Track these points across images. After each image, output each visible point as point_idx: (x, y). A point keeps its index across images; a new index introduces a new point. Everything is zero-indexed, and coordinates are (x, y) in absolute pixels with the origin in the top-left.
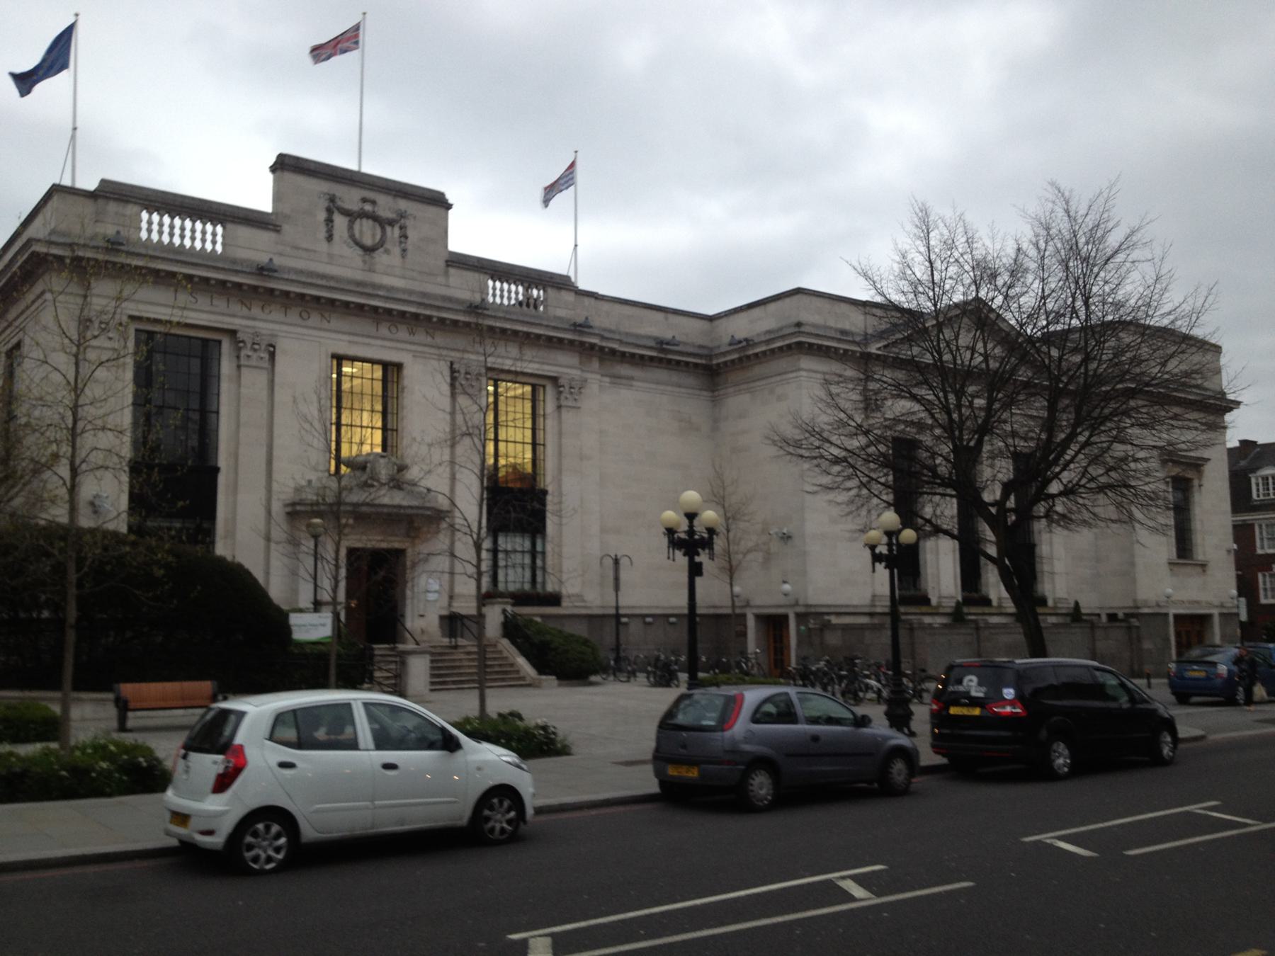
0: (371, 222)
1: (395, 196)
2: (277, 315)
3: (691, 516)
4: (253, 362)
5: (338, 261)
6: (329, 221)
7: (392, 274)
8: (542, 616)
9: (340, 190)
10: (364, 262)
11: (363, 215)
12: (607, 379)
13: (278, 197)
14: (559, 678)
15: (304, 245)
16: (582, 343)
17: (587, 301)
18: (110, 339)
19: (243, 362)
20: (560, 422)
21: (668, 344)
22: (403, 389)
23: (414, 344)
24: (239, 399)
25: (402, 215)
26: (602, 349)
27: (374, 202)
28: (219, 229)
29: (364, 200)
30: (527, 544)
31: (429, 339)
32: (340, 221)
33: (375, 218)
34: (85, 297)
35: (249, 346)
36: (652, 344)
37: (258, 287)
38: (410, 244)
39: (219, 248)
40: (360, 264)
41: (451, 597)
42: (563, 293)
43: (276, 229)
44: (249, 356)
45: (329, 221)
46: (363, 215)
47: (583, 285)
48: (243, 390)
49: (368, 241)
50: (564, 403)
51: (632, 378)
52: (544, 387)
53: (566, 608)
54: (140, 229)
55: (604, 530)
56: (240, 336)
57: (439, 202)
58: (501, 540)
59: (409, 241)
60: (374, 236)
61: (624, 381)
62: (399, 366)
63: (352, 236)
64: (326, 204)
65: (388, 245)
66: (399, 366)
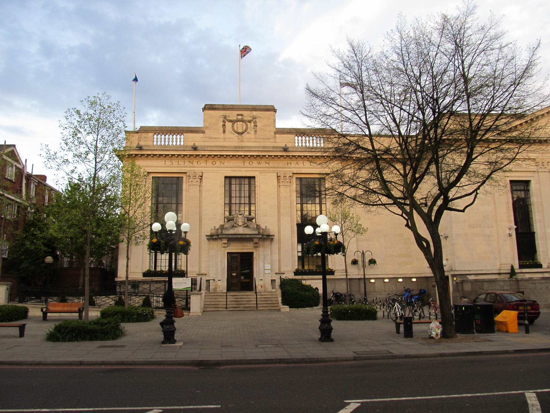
0: (241, 123)
5: (230, 140)
6: (224, 125)
7: (251, 141)
10: (239, 139)
16: (288, 156)
27: (242, 115)
29: (238, 115)
32: (229, 125)
33: (242, 121)
37: (194, 154)
43: (203, 132)
45: (224, 125)
49: (240, 131)
64: (223, 119)
65: (248, 131)
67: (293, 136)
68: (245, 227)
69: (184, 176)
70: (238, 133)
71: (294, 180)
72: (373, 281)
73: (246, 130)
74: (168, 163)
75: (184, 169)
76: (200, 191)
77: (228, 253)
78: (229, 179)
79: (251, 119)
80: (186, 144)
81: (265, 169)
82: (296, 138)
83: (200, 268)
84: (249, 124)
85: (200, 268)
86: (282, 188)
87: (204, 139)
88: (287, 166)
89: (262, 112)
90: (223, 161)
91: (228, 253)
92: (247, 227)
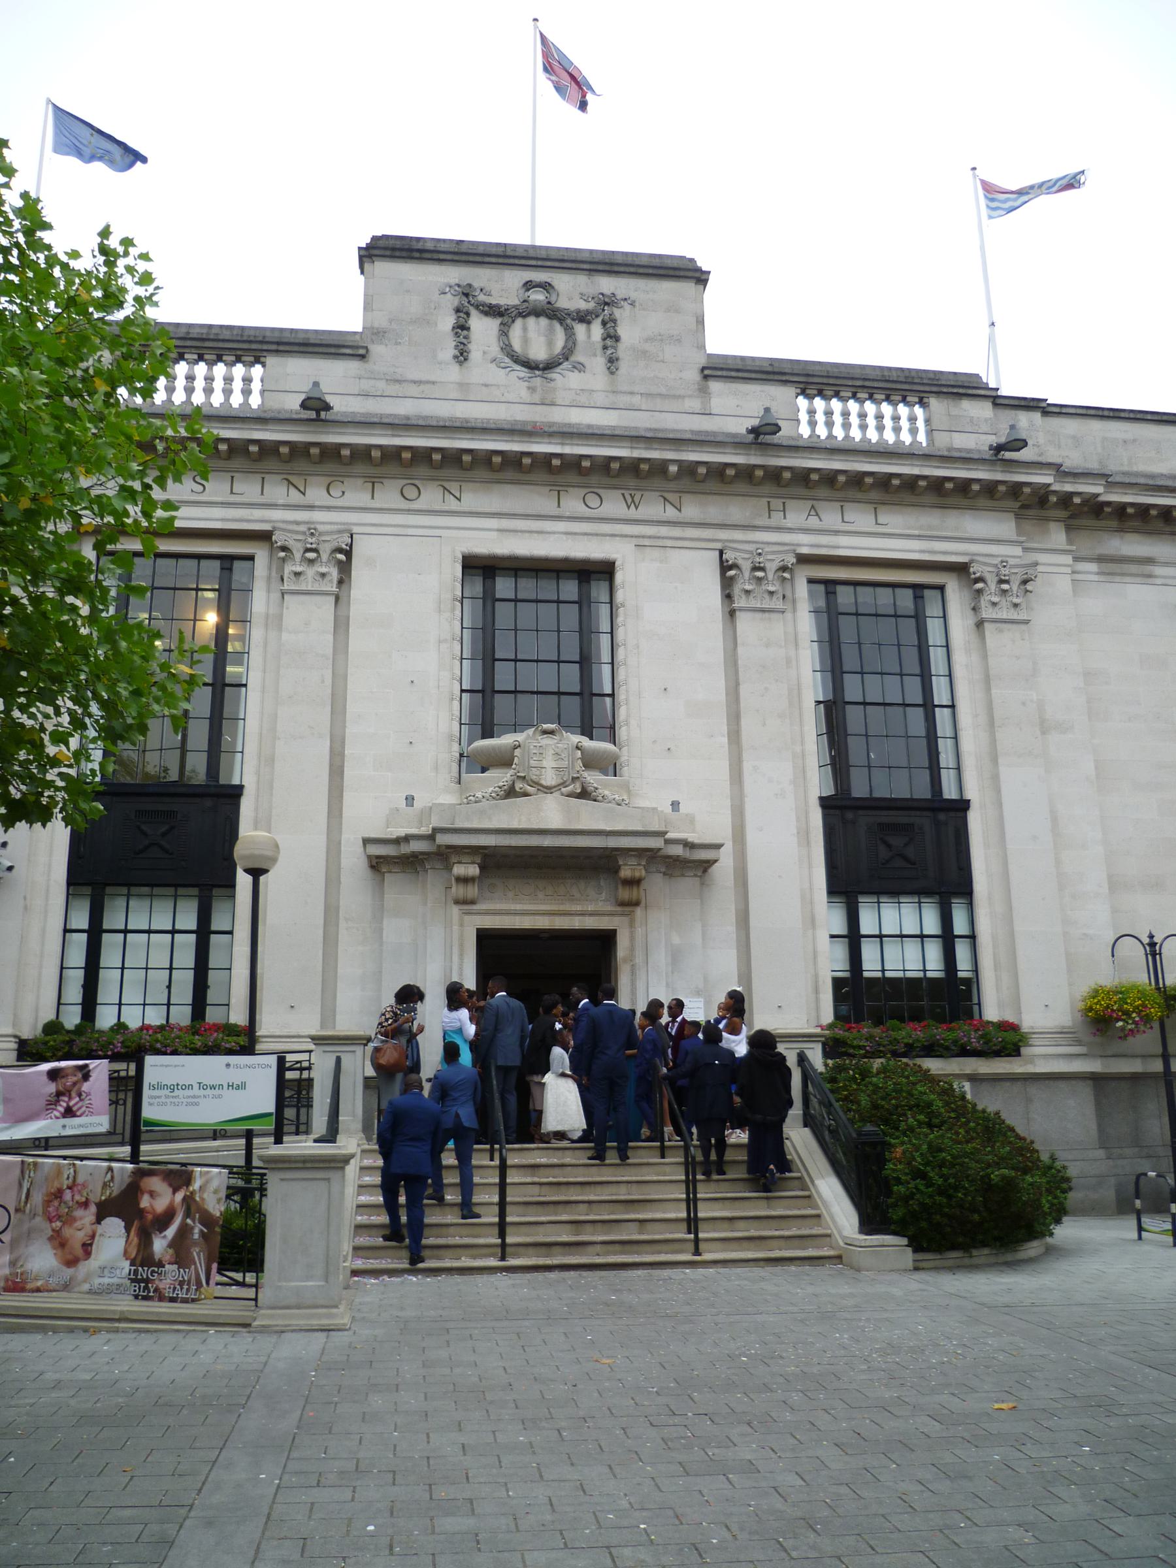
0: (543, 321)
2: (355, 494)
4: (307, 584)
5: (485, 394)
6: (461, 328)
7: (588, 403)
8: (973, 1078)
9: (479, 276)
10: (532, 389)
12: (1093, 567)
14: (918, 1245)
16: (1015, 490)
20: (984, 656)
25: (608, 302)
26: (1066, 500)
27: (546, 286)
29: (529, 285)
30: (931, 923)
31: (671, 513)
32: (483, 329)
33: (550, 312)
35: (298, 555)
37: (310, 450)
38: (623, 350)
40: (525, 394)
42: (966, 404)
43: (362, 356)
45: (461, 328)
49: (539, 353)
50: (987, 613)
51: (1150, 561)
52: (941, 588)
55: (1115, 884)
57: (690, 274)
58: (935, 965)
59: (621, 346)
60: (550, 344)
61: (1133, 568)
62: (605, 571)
63: (508, 350)
64: (456, 302)
65: (578, 357)
66: (605, 571)
67: (791, 391)
69: (261, 555)
70: (530, 365)
71: (802, 589)
73: (567, 354)
75: (258, 513)
76: (341, 625)
78: (481, 569)
79: (591, 305)
81: (664, 531)
82: (802, 402)
83: (328, 1013)
85: (328, 1013)
86: (743, 619)
89: (641, 283)
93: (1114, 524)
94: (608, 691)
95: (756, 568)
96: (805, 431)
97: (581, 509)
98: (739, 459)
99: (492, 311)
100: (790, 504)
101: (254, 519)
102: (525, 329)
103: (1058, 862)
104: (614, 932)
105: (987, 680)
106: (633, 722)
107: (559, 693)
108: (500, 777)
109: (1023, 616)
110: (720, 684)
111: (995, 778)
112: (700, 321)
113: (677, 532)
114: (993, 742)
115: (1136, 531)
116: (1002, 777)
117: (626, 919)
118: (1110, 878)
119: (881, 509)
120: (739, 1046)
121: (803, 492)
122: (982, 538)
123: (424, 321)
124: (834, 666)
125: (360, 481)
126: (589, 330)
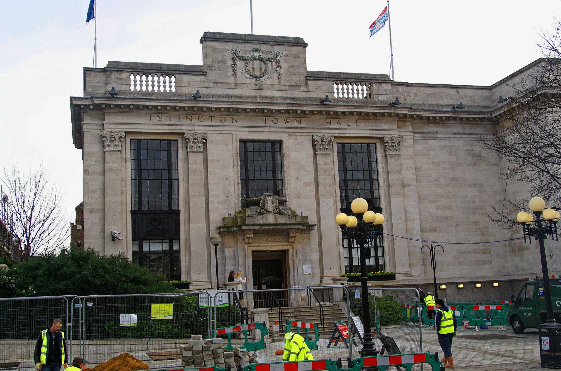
1: (272, 45)
3: (538, 214)
7: (274, 89)
10: (256, 85)
11: (253, 59)
12: (419, 135)
13: (205, 57)
15: (221, 81)
16: (397, 115)
17: (400, 88)
18: (117, 145)
19: (107, 148)
20: (387, 165)
21: (457, 108)
22: (283, 155)
23: (288, 128)
24: (188, 169)
26: (412, 116)
28: (173, 79)
29: (254, 50)
31: (298, 125)
33: (260, 59)
34: (103, 125)
36: (449, 109)
37: (192, 107)
39: (173, 89)
41: (322, 278)
42: (383, 85)
44: (192, 147)
46: (253, 59)
47: (397, 79)
48: (189, 165)
52: (375, 144)
53: (400, 280)
54: (130, 85)
55: (422, 230)
56: (186, 136)
57: (300, 43)
62: (280, 142)
66: (280, 142)
67: (331, 83)
68: (277, 213)
70: (256, 77)
72: (443, 287)
74: (155, 120)
75: (179, 127)
76: (206, 161)
77: (253, 252)
78: (244, 143)
80: (179, 91)
81: (296, 130)
84: (269, 64)
86: (320, 159)
87: (207, 84)
88: (325, 127)
90: (235, 118)
91: (253, 252)
92: (280, 213)
93: (426, 121)
94: (280, 178)
95: (322, 141)
96: (336, 95)
97: (273, 125)
98: (318, 109)
99: (243, 59)
100: (332, 120)
101: (178, 129)
102: (253, 64)
103: (407, 225)
104: (288, 250)
105: (388, 172)
106: (289, 189)
107: (267, 180)
108: (255, 209)
109: (398, 153)
110: (313, 176)
111: (389, 201)
112: (305, 60)
113: (300, 131)
114: (389, 191)
115: (432, 125)
116: (392, 201)
117: (291, 247)
118: (421, 228)
119: (358, 121)
120: (359, 246)
121: (336, 117)
122: (387, 130)
123: (223, 62)
124: (343, 169)
125: (208, 116)
126: (272, 64)
